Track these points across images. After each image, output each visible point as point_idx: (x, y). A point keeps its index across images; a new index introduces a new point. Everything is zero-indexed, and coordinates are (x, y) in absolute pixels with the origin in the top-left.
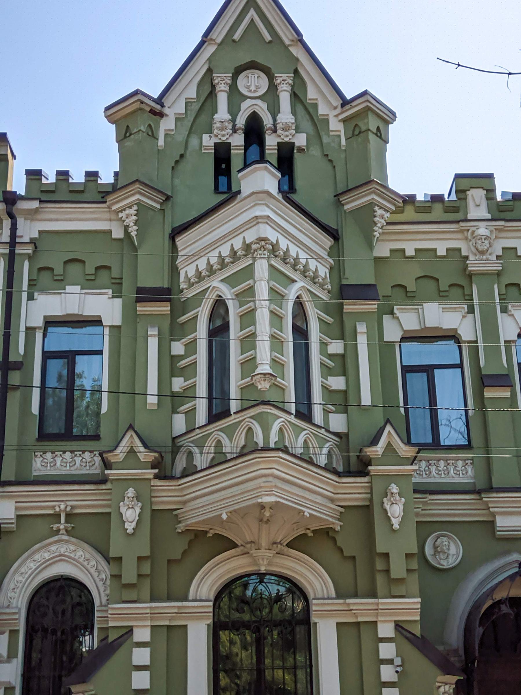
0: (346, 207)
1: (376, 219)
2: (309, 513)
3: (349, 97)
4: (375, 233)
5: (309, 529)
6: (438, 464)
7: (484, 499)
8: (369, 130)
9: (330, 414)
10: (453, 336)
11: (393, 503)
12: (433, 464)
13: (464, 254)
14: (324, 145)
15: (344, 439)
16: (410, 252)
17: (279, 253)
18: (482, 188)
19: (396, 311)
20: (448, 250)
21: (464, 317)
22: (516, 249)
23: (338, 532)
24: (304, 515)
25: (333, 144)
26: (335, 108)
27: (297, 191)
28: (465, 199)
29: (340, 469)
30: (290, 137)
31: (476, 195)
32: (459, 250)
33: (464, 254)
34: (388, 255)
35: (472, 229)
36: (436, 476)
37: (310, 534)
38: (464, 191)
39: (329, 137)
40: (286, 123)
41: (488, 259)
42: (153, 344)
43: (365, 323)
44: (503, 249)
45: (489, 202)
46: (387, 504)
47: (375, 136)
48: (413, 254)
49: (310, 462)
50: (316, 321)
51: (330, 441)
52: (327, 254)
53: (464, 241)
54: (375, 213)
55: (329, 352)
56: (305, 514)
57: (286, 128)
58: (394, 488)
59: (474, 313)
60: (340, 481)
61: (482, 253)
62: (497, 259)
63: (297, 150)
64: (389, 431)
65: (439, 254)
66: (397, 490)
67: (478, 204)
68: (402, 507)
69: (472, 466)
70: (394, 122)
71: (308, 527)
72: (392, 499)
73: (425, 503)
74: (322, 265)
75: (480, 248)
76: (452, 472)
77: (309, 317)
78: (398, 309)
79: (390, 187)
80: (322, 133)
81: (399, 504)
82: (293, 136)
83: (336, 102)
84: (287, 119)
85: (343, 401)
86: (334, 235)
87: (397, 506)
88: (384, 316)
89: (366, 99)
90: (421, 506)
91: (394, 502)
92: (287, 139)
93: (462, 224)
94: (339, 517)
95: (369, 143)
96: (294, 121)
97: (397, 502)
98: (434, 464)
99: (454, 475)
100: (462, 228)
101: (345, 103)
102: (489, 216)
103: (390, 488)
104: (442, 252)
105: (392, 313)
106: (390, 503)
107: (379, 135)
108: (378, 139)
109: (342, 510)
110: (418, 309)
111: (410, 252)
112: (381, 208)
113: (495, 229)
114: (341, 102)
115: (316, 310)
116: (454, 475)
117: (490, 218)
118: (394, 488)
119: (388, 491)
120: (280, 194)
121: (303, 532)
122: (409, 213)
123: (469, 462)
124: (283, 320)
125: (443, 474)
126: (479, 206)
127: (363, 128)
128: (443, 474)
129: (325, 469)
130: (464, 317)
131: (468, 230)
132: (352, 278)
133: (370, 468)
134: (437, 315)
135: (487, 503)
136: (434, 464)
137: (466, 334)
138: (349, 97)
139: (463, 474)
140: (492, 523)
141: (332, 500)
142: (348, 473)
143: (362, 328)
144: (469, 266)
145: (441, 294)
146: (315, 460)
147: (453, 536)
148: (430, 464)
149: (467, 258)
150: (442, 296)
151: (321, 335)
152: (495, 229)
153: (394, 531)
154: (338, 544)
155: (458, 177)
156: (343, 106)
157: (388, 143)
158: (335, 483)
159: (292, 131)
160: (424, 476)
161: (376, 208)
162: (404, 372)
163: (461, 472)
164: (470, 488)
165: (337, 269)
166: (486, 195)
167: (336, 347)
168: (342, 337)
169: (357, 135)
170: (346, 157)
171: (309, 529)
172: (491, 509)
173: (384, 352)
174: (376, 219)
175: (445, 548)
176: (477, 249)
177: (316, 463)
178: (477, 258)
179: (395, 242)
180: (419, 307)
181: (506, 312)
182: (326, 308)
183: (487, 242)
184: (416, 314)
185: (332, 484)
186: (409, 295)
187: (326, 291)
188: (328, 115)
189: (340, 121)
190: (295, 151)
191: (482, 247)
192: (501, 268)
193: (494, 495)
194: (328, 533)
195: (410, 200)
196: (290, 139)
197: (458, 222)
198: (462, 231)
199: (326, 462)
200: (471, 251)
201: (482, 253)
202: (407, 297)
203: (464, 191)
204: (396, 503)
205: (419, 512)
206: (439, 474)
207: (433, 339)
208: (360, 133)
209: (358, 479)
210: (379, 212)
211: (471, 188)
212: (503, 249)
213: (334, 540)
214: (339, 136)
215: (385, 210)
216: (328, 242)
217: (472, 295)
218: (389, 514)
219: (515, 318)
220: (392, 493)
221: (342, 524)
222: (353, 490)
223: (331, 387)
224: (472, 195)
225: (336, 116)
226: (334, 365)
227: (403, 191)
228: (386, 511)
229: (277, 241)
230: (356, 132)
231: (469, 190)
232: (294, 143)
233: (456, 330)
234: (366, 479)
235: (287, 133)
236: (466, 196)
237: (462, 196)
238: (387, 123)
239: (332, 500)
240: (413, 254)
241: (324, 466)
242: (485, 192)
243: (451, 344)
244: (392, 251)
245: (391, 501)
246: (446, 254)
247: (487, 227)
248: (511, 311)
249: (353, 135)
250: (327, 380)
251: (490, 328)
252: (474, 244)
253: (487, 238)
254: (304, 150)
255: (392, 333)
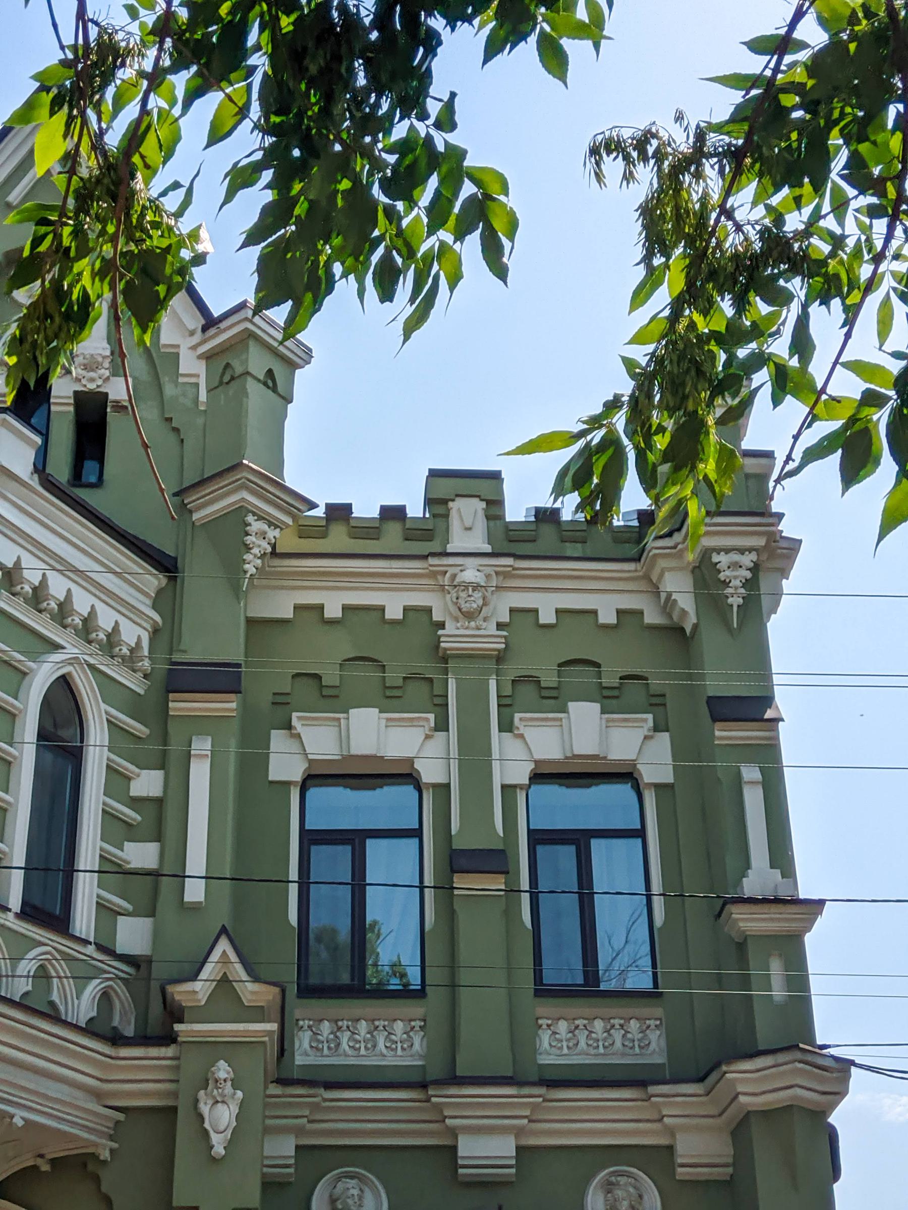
0: (195, 516)
1: (249, 539)
2: (22, 1118)
3: (216, 314)
4: (247, 566)
5: (41, 1156)
6: (357, 1029)
7: (434, 1099)
8: (248, 373)
9: (119, 917)
10: (404, 775)
11: (217, 1102)
12: (345, 1028)
13: (437, 617)
14: (165, 402)
15: (143, 966)
16: (333, 611)
17: (22, 588)
18: (478, 496)
19: (295, 722)
20: (406, 609)
21: (427, 737)
22: (536, 611)
23: (105, 1162)
24: (11, 1124)
25: (182, 400)
26: (192, 333)
27: (105, 483)
28: (446, 516)
29: (129, 1031)
30: (100, 382)
31: (467, 512)
32: (428, 611)
33: (437, 617)
34: (291, 615)
35: (451, 571)
36: (350, 1052)
37: (45, 1168)
38: (445, 502)
39: (176, 386)
40: (92, 355)
41: (478, 629)
42: (197, 860)
43: (210, 739)
44: (512, 610)
45: (492, 523)
46: (206, 1103)
47: (261, 385)
48: (339, 614)
49: (53, 1015)
50: (102, 730)
51: (109, 973)
52: (149, 602)
53: (439, 594)
54: (248, 528)
55: (131, 794)
56: (14, 1120)
57: (91, 365)
58: (223, 1070)
59: (448, 730)
60: (113, 1054)
61: (469, 616)
62: (498, 629)
63: (113, 407)
64: (224, 951)
65: (388, 616)
66: (228, 1073)
67: (468, 524)
68: (235, 1109)
69: (422, 1033)
70: (307, 366)
71: (42, 1152)
72: (215, 1091)
73: (315, 1107)
74: (130, 619)
75: (465, 607)
76: (345, 1045)
77: (87, 720)
78: (299, 718)
79: (289, 483)
80: (165, 380)
81: (230, 1102)
82: (107, 379)
83: (195, 321)
84: (96, 348)
85: (150, 890)
86: (165, 564)
87: (226, 1106)
88: (274, 733)
89: (243, 317)
90: (307, 1113)
91: (219, 1099)
92: (92, 386)
93: (432, 561)
94: (112, 1132)
95: (247, 397)
96: (108, 353)
97: (226, 1099)
98: (348, 1027)
99: (385, 1051)
100: (435, 569)
101: (210, 322)
102: (488, 548)
103: (213, 1069)
104: (394, 612)
105: (289, 726)
106: (210, 1102)
107: (270, 384)
108: (270, 392)
109: (121, 1117)
110: (339, 719)
111: (333, 611)
112: (260, 518)
113: (497, 573)
114: (203, 322)
115: (103, 706)
116: (385, 1051)
117: (490, 551)
118: (223, 1070)
119: (210, 1074)
120: (36, 476)
121: (30, 1163)
122: (338, 538)
123: (417, 1024)
124: (17, 718)
125: (363, 1048)
126: (470, 529)
127: (239, 370)
128: (363, 1048)
129: (90, 1030)
130: (427, 737)
131: (446, 572)
132: (196, 649)
133: (177, 1027)
134: (372, 732)
135: (439, 1108)
136: (348, 1027)
137: (430, 772)
138: (216, 314)
139: (329, 1048)
140: (454, 1149)
141: (97, 1095)
142: (143, 1039)
143: (202, 746)
144: (442, 639)
145: (389, 693)
146: (62, 1008)
147: (370, 1176)
148: (339, 1028)
149: (442, 625)
150: (390, 698)
151: (113, 757)
152: (497, 573)
153: (214, 1160)
154: (104, 1188)
155: (434, 474)
156: (204, 329)
157: (291, 402)
158: (103, 1058)
159: (103, 371)
160: (326, 1051)
161: (250, 518)
162: (306, 841)
163: (399, 1045)
164: (415, 1077)
165: (164, 635)
166: (485, 510)
167: (148, 783)
168: (162, 764)
169: (227, 383)
170: (205, 425)
171: (41, 1156)
172: (448, 1122)
173: (250, 795)
174: (249, 539)
175: (350, 1201)
176: (460, 609)
177: (63, 1018)
178: (459, 625)
179: (304, 592)
180: (341, 715)
181: (511, 731)
182: (134, 705)
183: (477, 595)
184: (337, 729)
185: (94, 1059)
186: (325, 692)
187: (139, 675)
188: (178, 346)
189: (199, 357)
190: (109, 410)
191: (467, 605)
192: (503, 646)
193: (453, 1091)
194: (85, 1165)
195: (339, 513)
196: (98, 386)
197: (425, 557)
198: (433, 575)
199: (94, 1014)
200: (451, 614)
201: (469, 616)
202: (323, 696)
203: (445, 502)
204: (223, 1102)
205: (304, 1126)
206: (355, 1049)
207: (379, 781)
208: (233, 378)
209: (154, 1051)
210: (256, 526)
211: (457, 496)
212: (512, 610)
213: (97, 1180)
214: (197, 385)
215: (270, 524)
216: (154, 580)
217: (447, 696)
218: (207, 1125)
219: (526, 744)
220: (217, 1081)
221: (115, 1145)
222: (142, 1075)
223: (129, 863)
224: (459, 509)
225: (194, 348)
226: (139, 818)
227: (323, 495)
228: (201, 1118)
229: (18, 563)
230: (227, 378)
231: (453, 500)
232: (106, 394)
233: (410, 761)
234: (170, 1051)
235: (92, 374)
236: (449, 510)
237: (440, 510)
238: (292, 366)
239: (97, 1095)
240: (339, 614)
241: (84, 1026)
242: (483, 505)
243: (625, 790)
244: (297, 608)
245: (214, 1097)
246: (401, 617)
247: (480, 568)
248: (518, 728)
249: (221, 383)
250: (122, 851)
251: (475, 759)
252: (455, 600)
253: (476, 587)
254: (126, 407)
255: (285, 765)
